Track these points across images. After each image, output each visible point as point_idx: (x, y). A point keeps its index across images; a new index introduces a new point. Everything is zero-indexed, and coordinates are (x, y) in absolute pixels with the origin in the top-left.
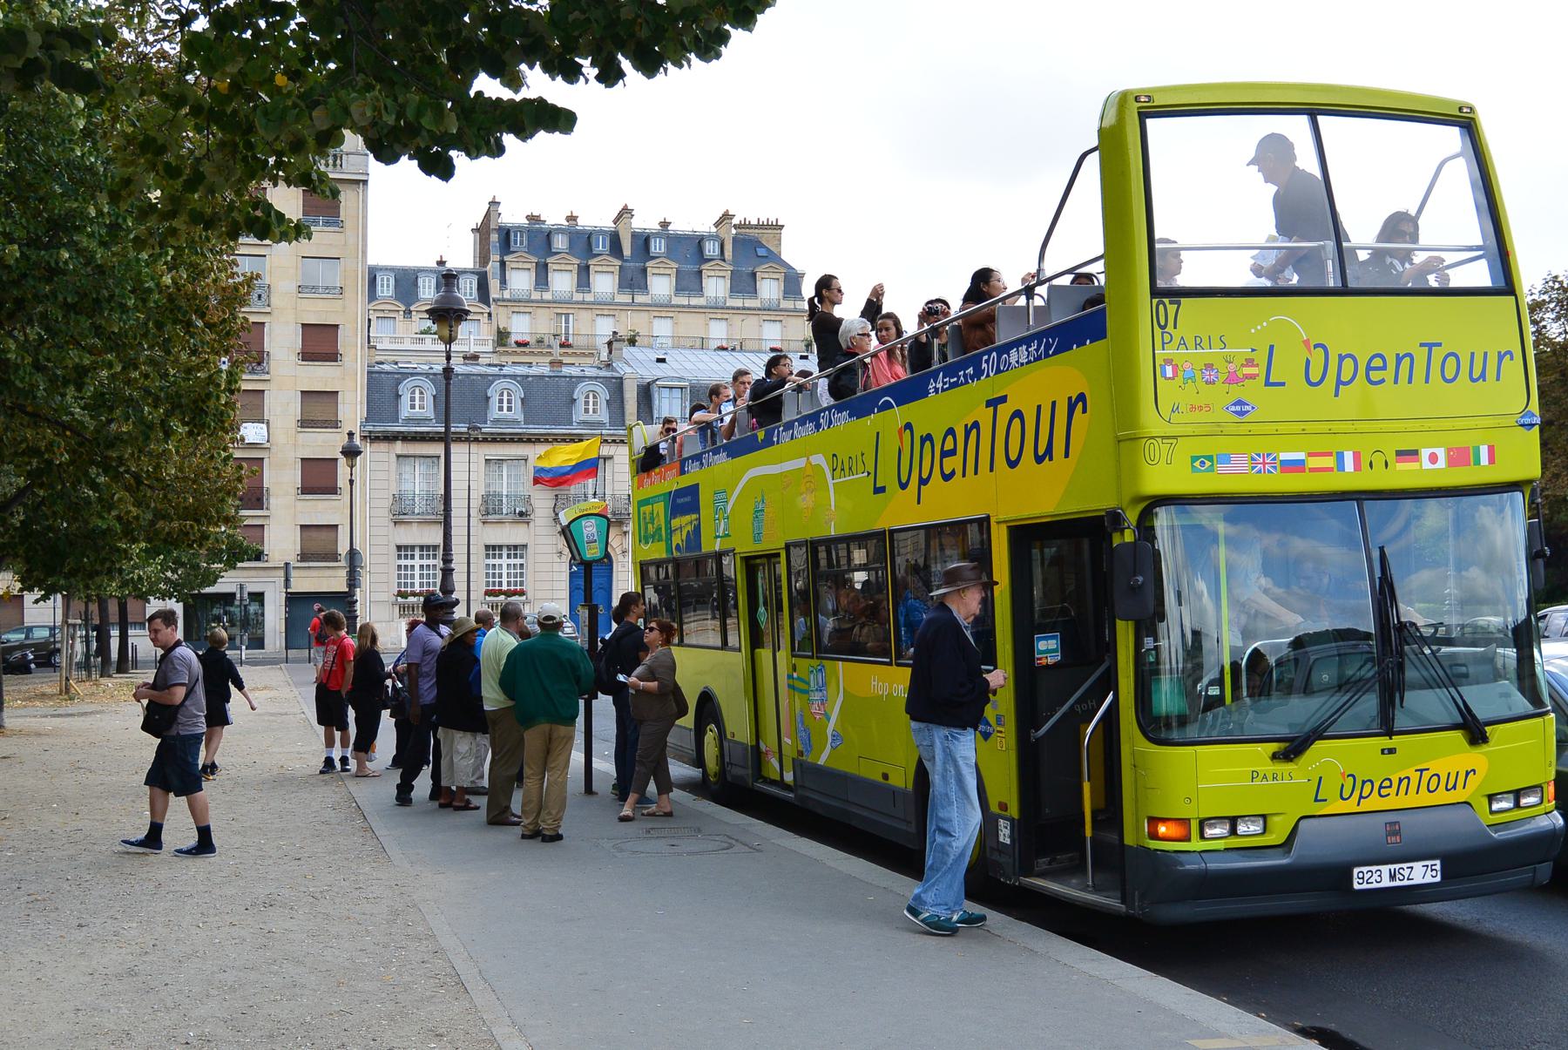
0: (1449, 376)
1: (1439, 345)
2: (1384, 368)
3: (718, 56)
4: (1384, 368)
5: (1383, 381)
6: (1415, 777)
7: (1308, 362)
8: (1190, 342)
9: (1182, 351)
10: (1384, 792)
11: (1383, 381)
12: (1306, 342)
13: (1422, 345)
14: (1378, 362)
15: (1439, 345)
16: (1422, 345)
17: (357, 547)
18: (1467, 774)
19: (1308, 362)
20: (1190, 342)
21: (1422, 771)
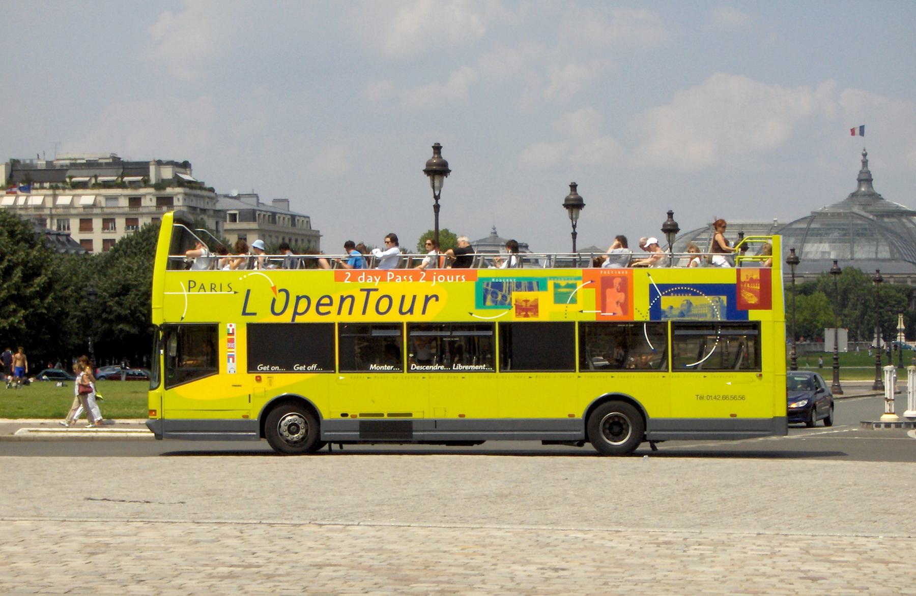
0: (386, 300)
1: (376, 290)
2: (331, 304)
3: (6, 164)
4: (331, 304)
5: (328, 313)
6: (360, 298)
7: (274, 300)
8: (207, 287)
9: (202, 292)
10: (323, 309)
11: (328, 313)
12: (274, 288)
13: (362, 290)
14: (326, 301)
15: (376, 290)
16: (362, 290)
17: (201, 544)
18: (427, 299)
19: (274, 300)
20: (207, 287)
21: (368, 291)
